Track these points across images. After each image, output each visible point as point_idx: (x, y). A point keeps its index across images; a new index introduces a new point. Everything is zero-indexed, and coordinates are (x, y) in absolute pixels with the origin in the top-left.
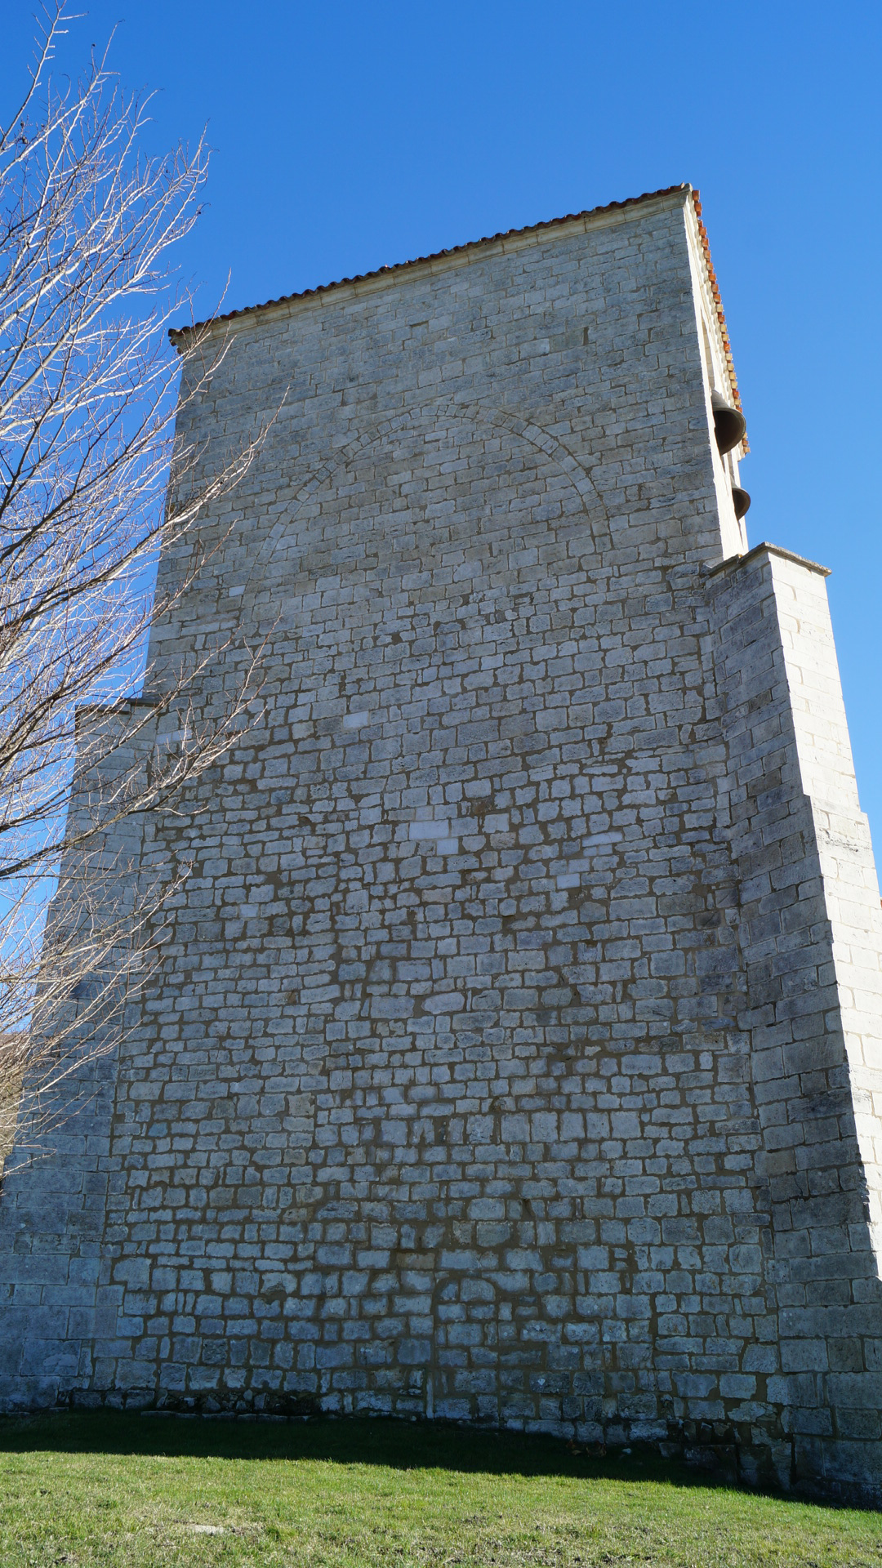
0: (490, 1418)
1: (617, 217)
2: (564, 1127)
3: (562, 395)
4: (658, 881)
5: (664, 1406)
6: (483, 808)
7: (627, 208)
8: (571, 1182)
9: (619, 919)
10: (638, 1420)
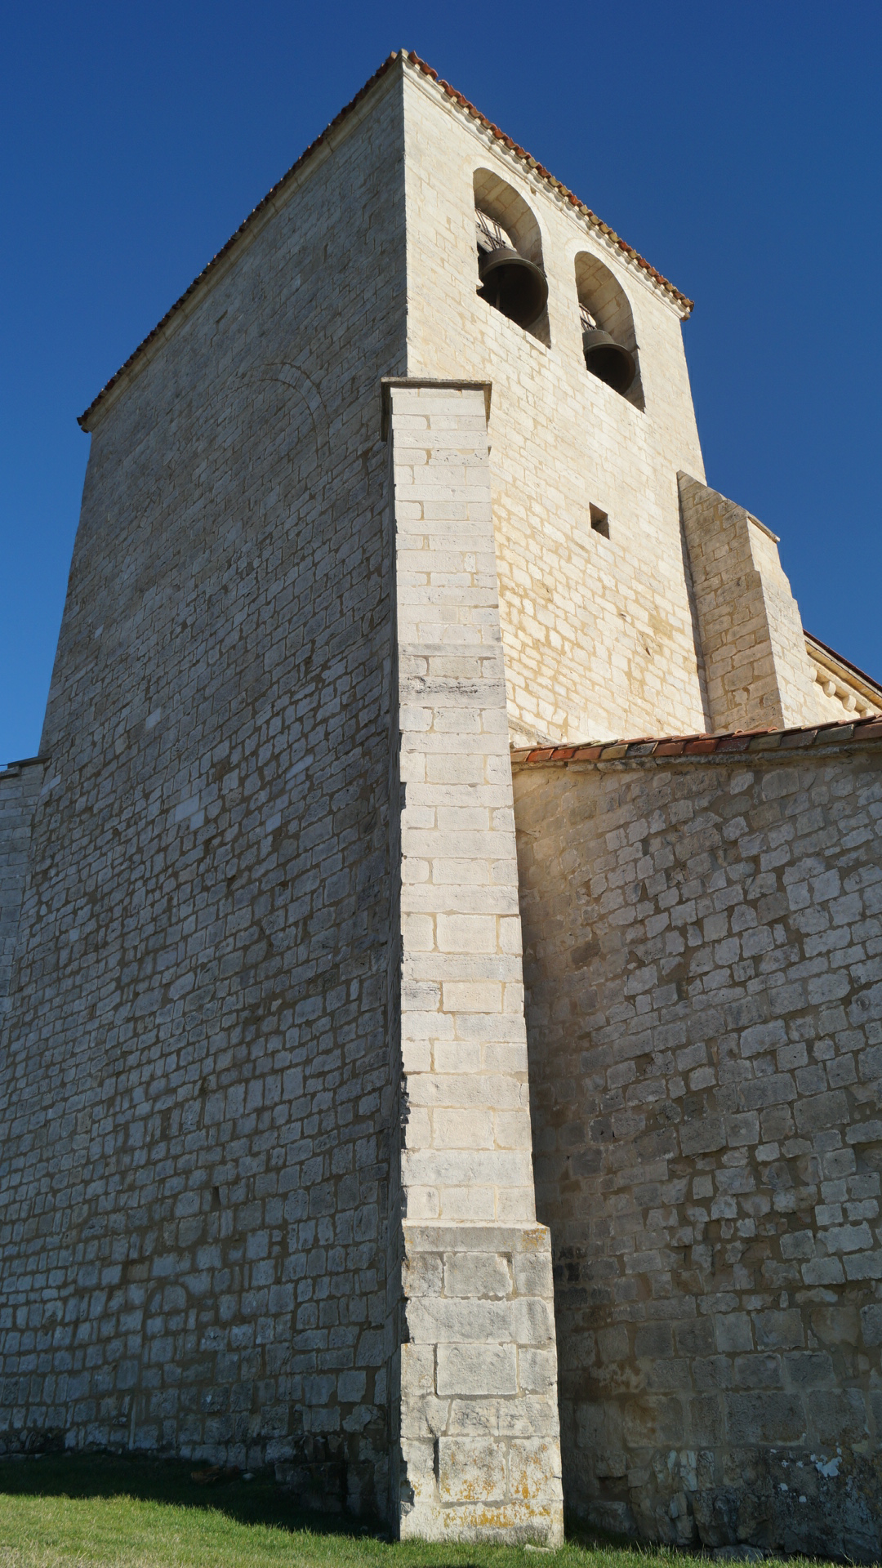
0: (169, 1446)
1: (353, 120)
2: (249, 1098)
3: (305, 323)
4: (337, 795)
5: (295, 1419)
6: (223, 768)
7: (357, 107)
8: (249, 1159)
9: (306, 851)
10: (272, 1438)
